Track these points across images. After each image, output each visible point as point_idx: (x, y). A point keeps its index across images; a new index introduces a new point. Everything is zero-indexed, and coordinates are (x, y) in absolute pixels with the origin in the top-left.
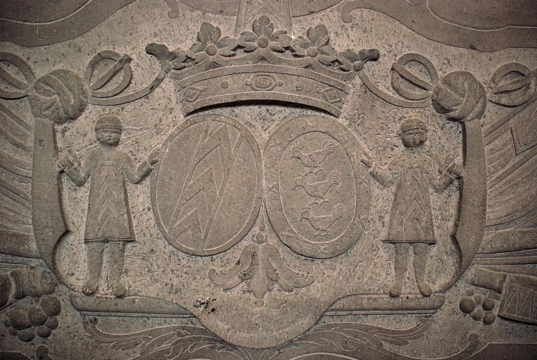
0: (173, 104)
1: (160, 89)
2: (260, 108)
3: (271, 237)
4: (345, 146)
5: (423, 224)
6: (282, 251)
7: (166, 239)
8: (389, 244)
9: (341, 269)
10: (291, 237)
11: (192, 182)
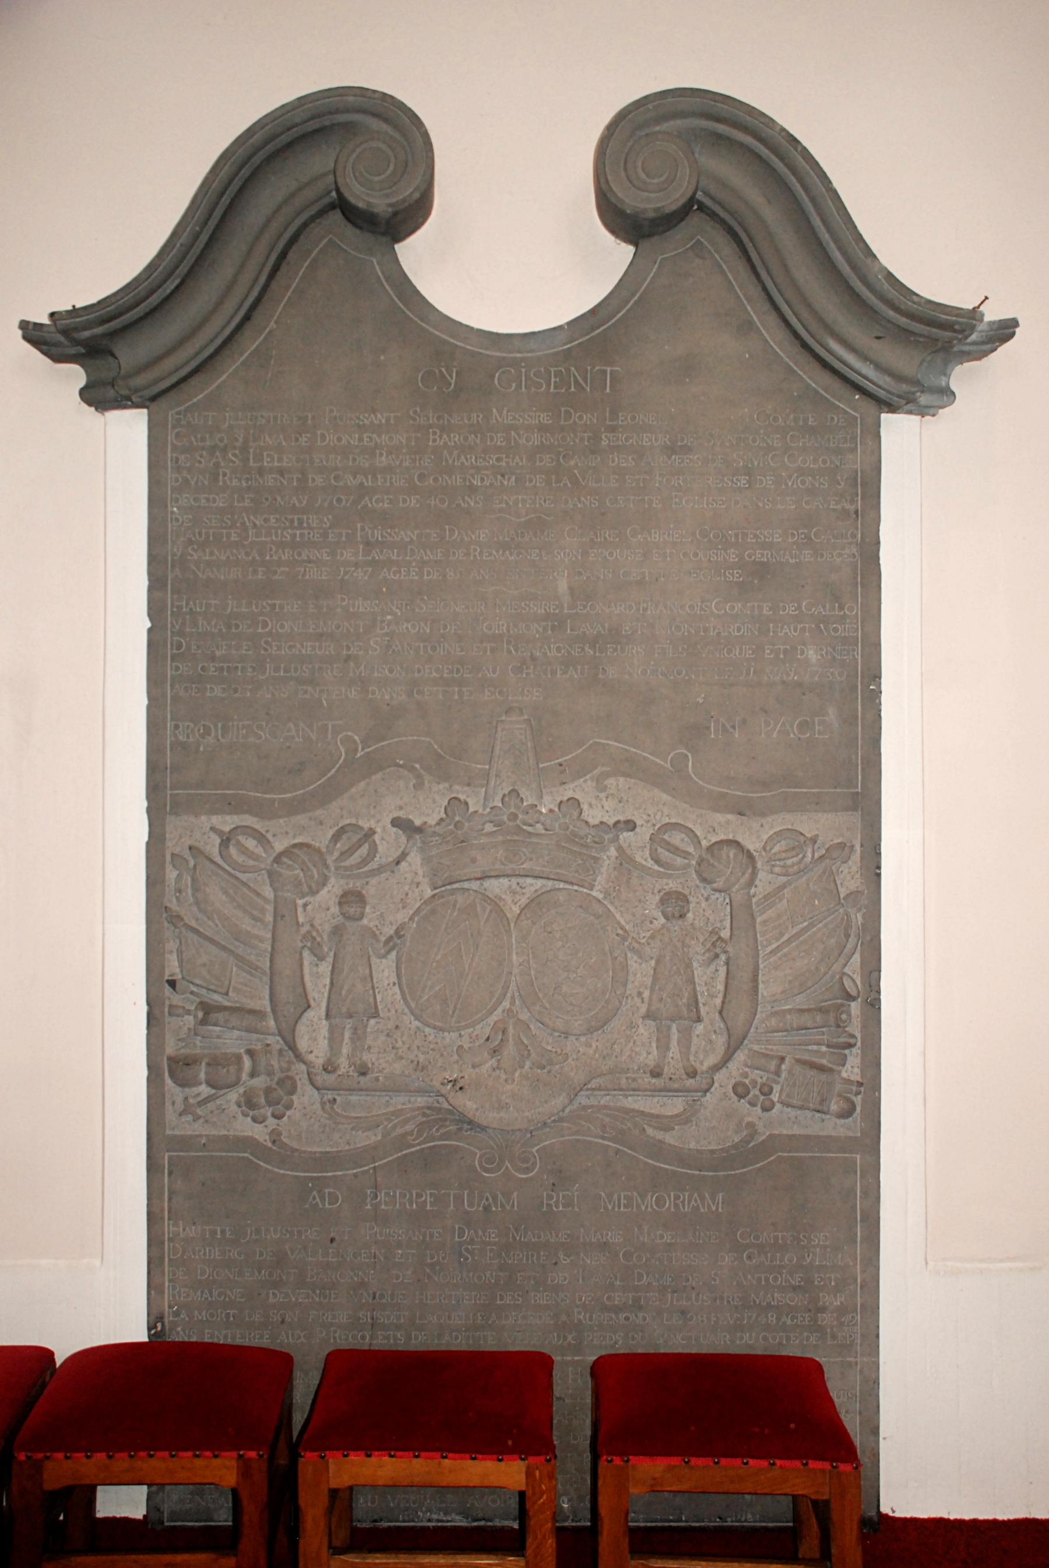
0: (420, 878)
5: (685, 1000)
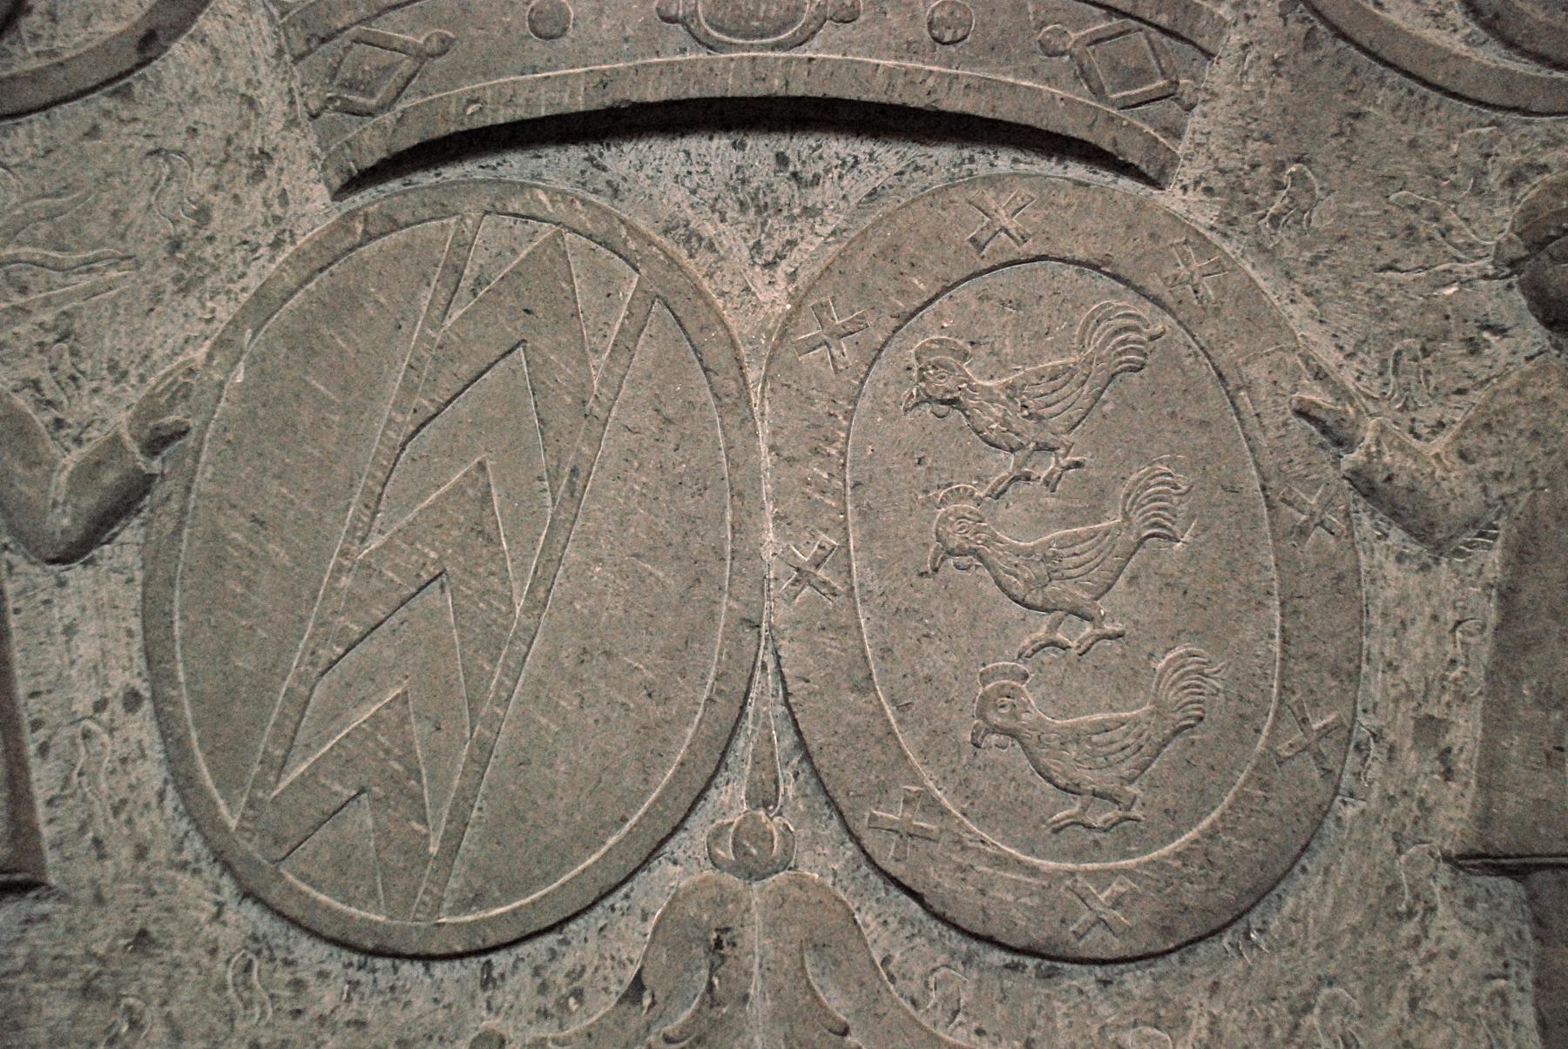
1: (196, 49)
2: (742, 146)
3: (814, 841)
4: (1208, 332)
6: (880, 923)
7: (227, 867)
8: (1490, 881)
9: (1214, 1020)
10: (926, 836)
11: (375, 542)
